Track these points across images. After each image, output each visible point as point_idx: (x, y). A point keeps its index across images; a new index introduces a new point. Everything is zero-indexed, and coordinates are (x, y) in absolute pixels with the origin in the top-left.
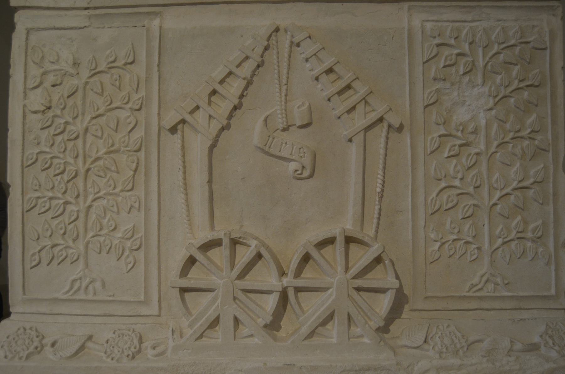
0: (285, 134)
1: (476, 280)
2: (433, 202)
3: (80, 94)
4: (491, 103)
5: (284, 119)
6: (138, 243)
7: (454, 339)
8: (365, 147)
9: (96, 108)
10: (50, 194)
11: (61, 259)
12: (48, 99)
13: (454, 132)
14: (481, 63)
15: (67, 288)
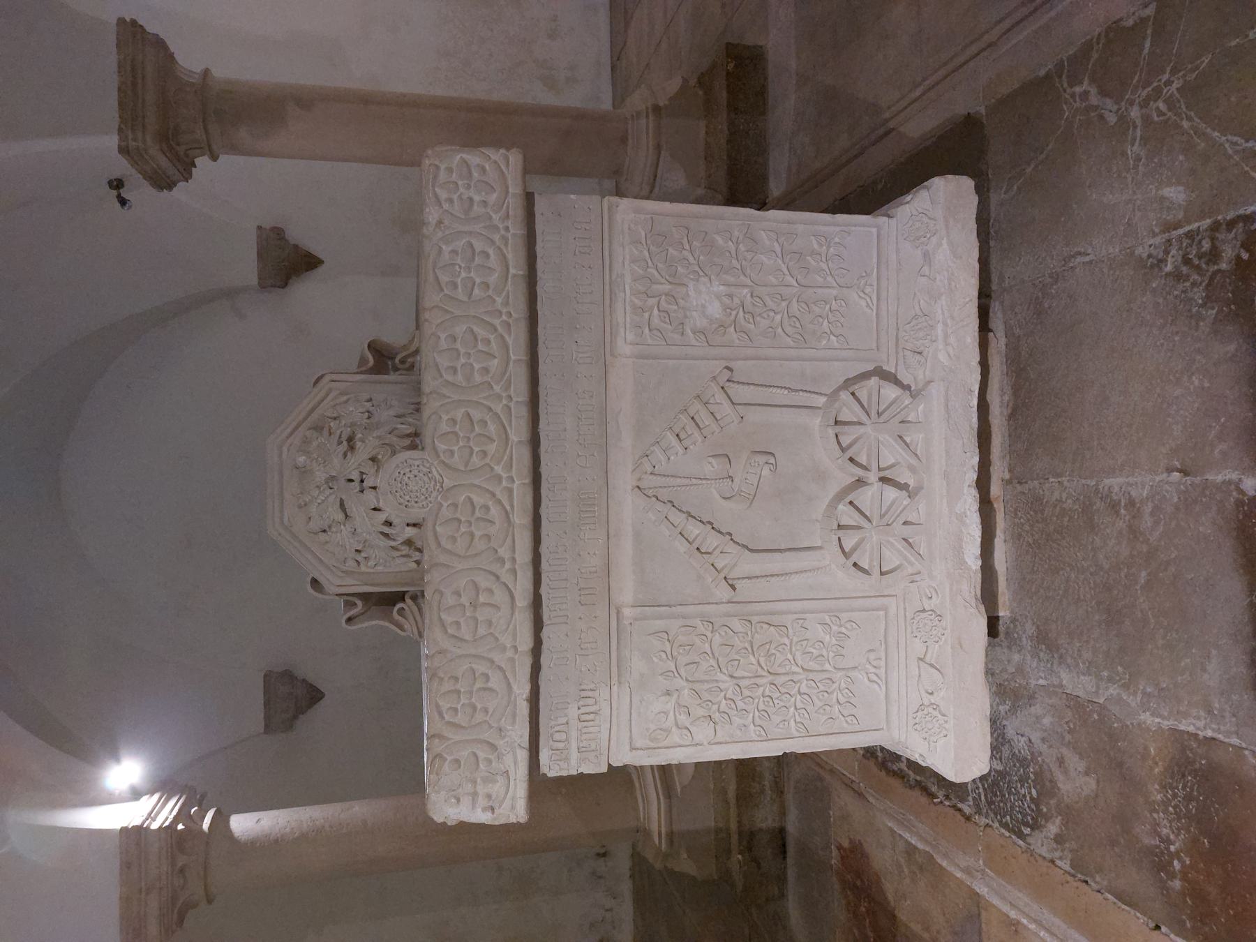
0: (735, 480)
1: (863, 303)
2: (796, 340)
3: (697, 686)
4: (705, 279)
5: (725, 480)
6: (833, 619)
7: (919, 327)
8: (759, 405)
9: (712, 668)
10: (792, 709)
11: (850, 694)
12: (702, 719)
13: (732, 318)
14: (667, 287)
15: (876, 686)
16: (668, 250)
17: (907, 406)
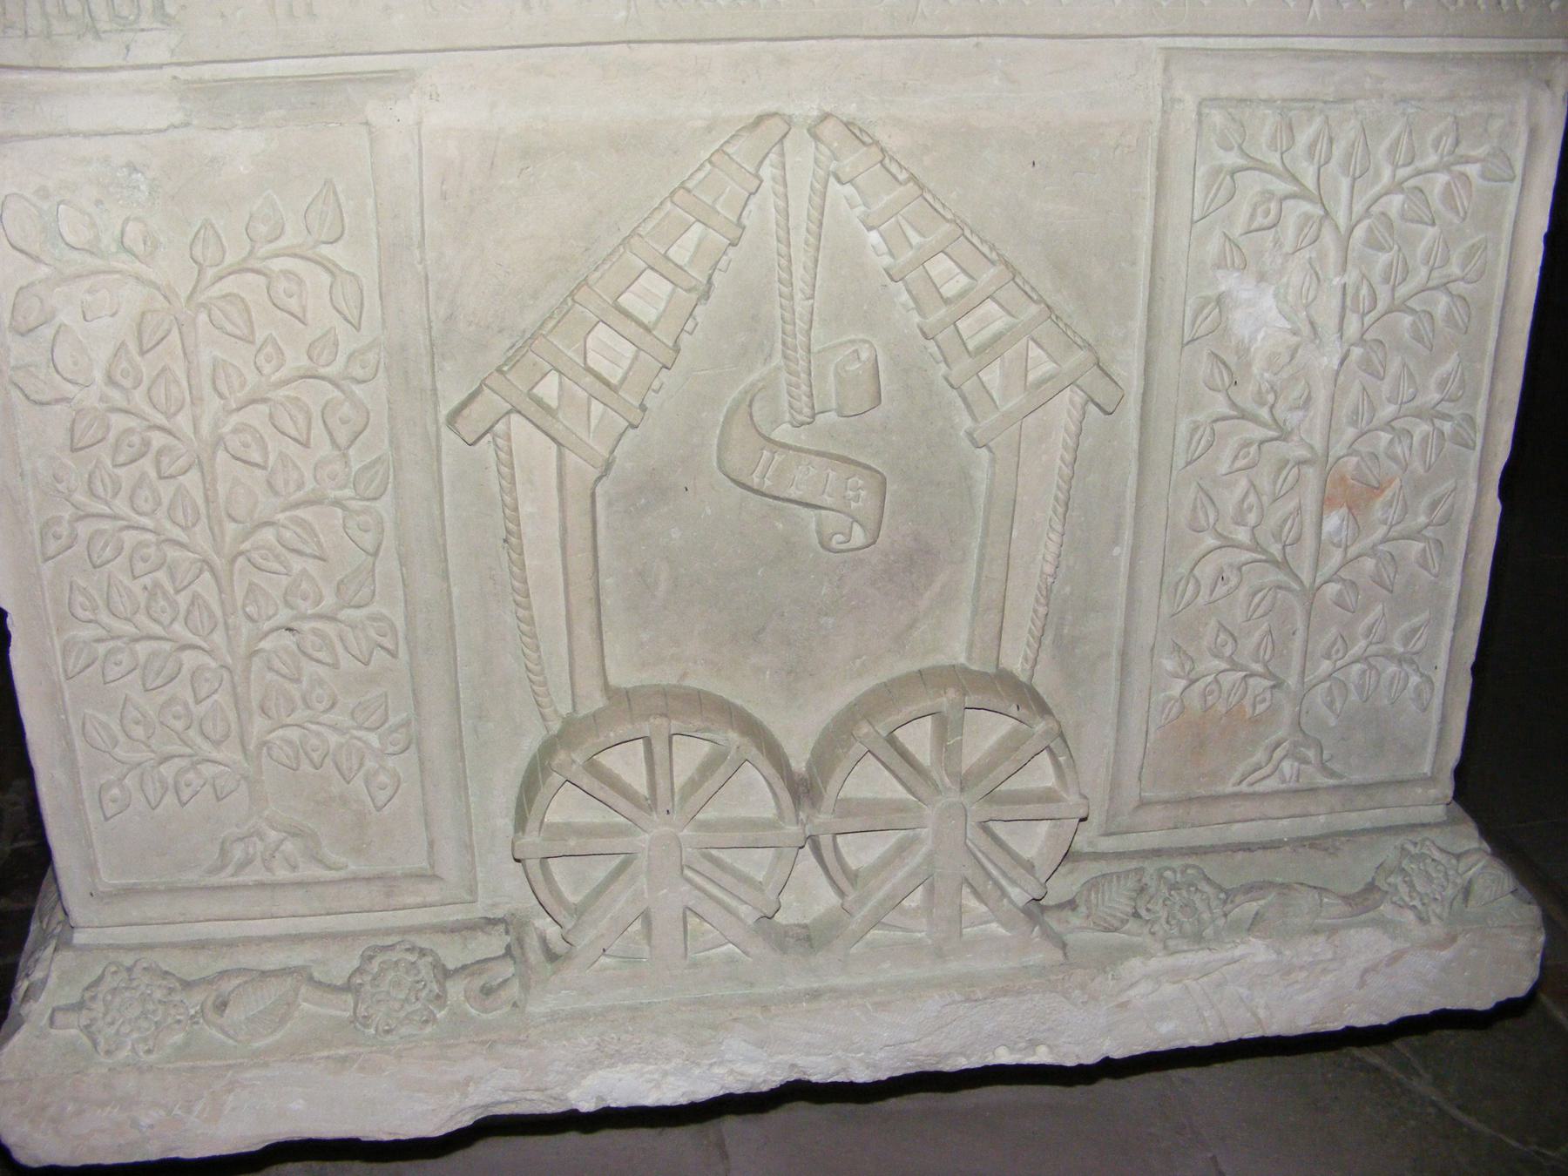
16: (1433, 224)
17: (1004, 894)
